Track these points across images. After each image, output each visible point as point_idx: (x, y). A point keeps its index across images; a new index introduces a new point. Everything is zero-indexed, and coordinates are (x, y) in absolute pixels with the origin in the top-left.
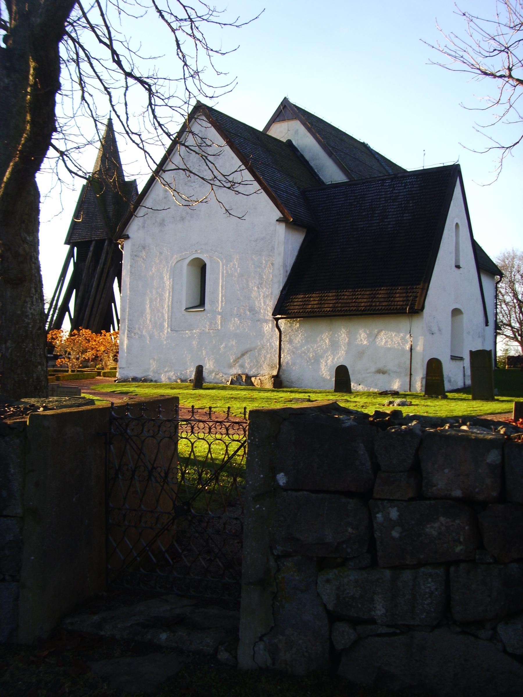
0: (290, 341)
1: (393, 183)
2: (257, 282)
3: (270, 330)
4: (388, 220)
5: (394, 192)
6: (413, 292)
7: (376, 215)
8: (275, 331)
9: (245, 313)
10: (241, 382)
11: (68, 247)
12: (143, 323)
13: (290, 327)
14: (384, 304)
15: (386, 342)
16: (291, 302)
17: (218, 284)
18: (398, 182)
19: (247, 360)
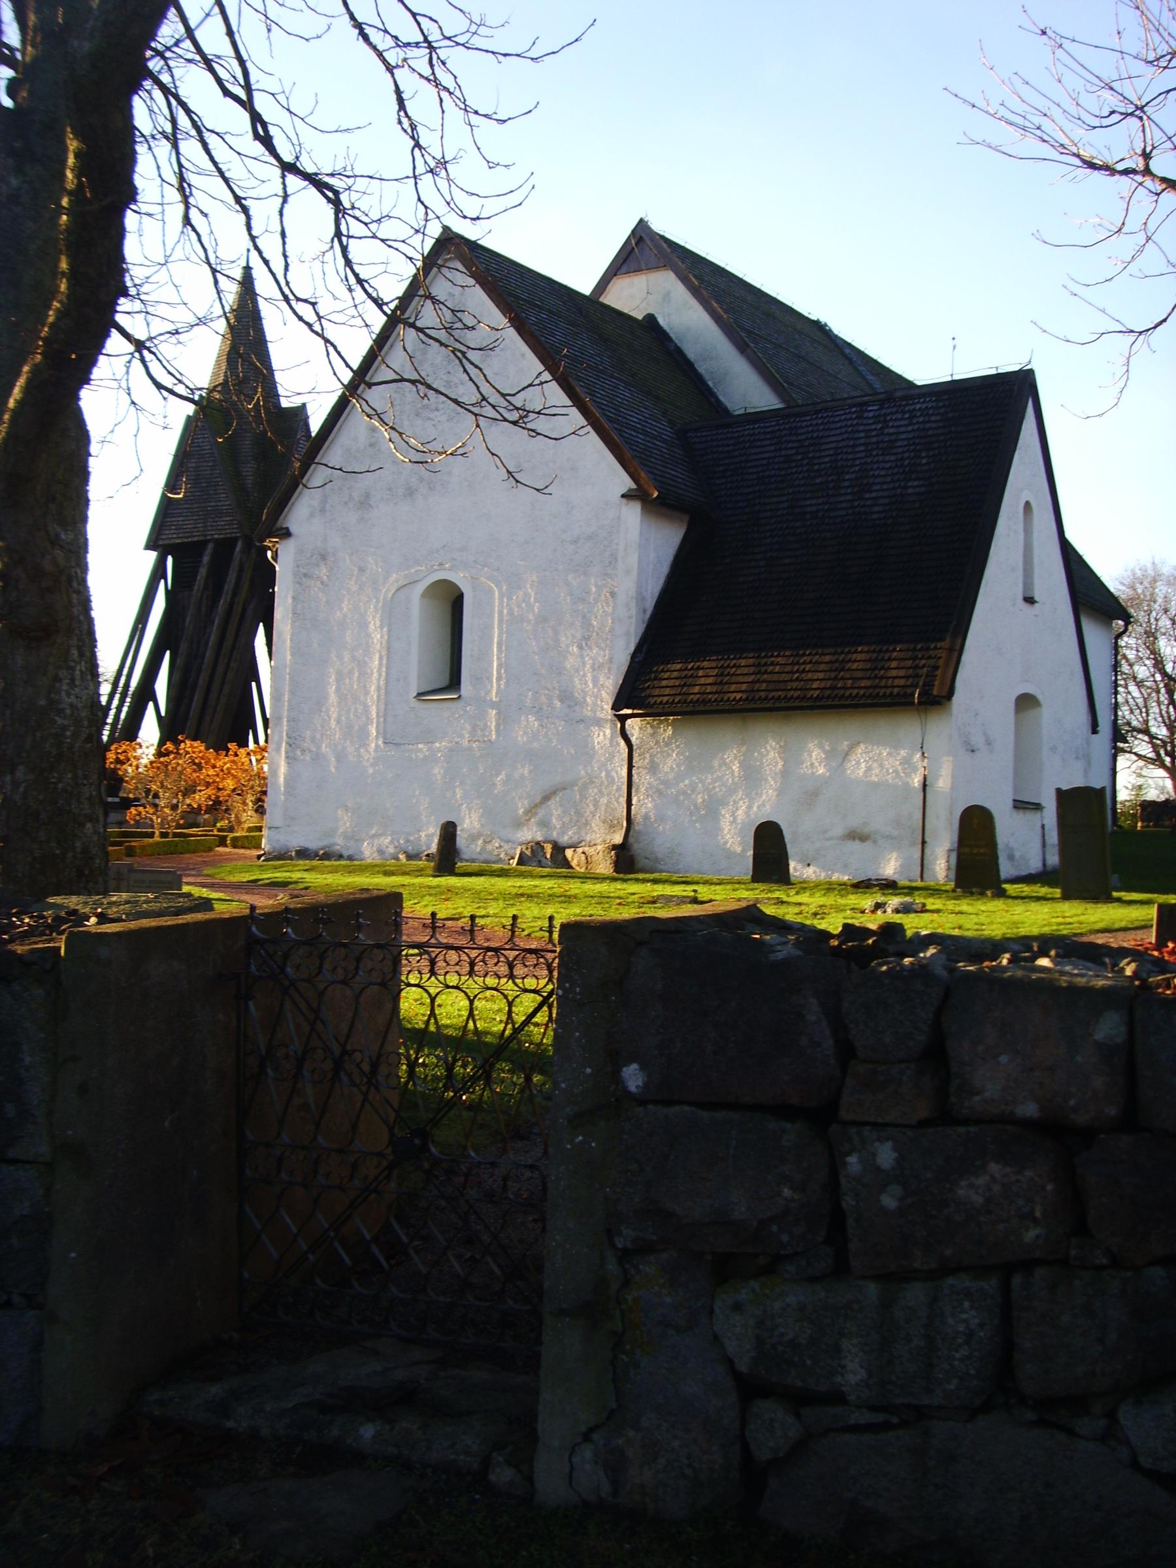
0: (653, 768)
1: (883, 412)
2: (579, 635)
3: (607, 742)
4: (873, 495)
5: (886, 431)
6: (929, 658)
7: (846, 484)
8: (618, 744)
9: (550, 705)
10: (543, 859)
11: (153, 555)
12: (322, 726)
13: (652, 735)
14: (864, 683)
15: (869, 769)
16: (655, 679)
17: (491, 638)
18: (894, 410)
19: (554, 810)
